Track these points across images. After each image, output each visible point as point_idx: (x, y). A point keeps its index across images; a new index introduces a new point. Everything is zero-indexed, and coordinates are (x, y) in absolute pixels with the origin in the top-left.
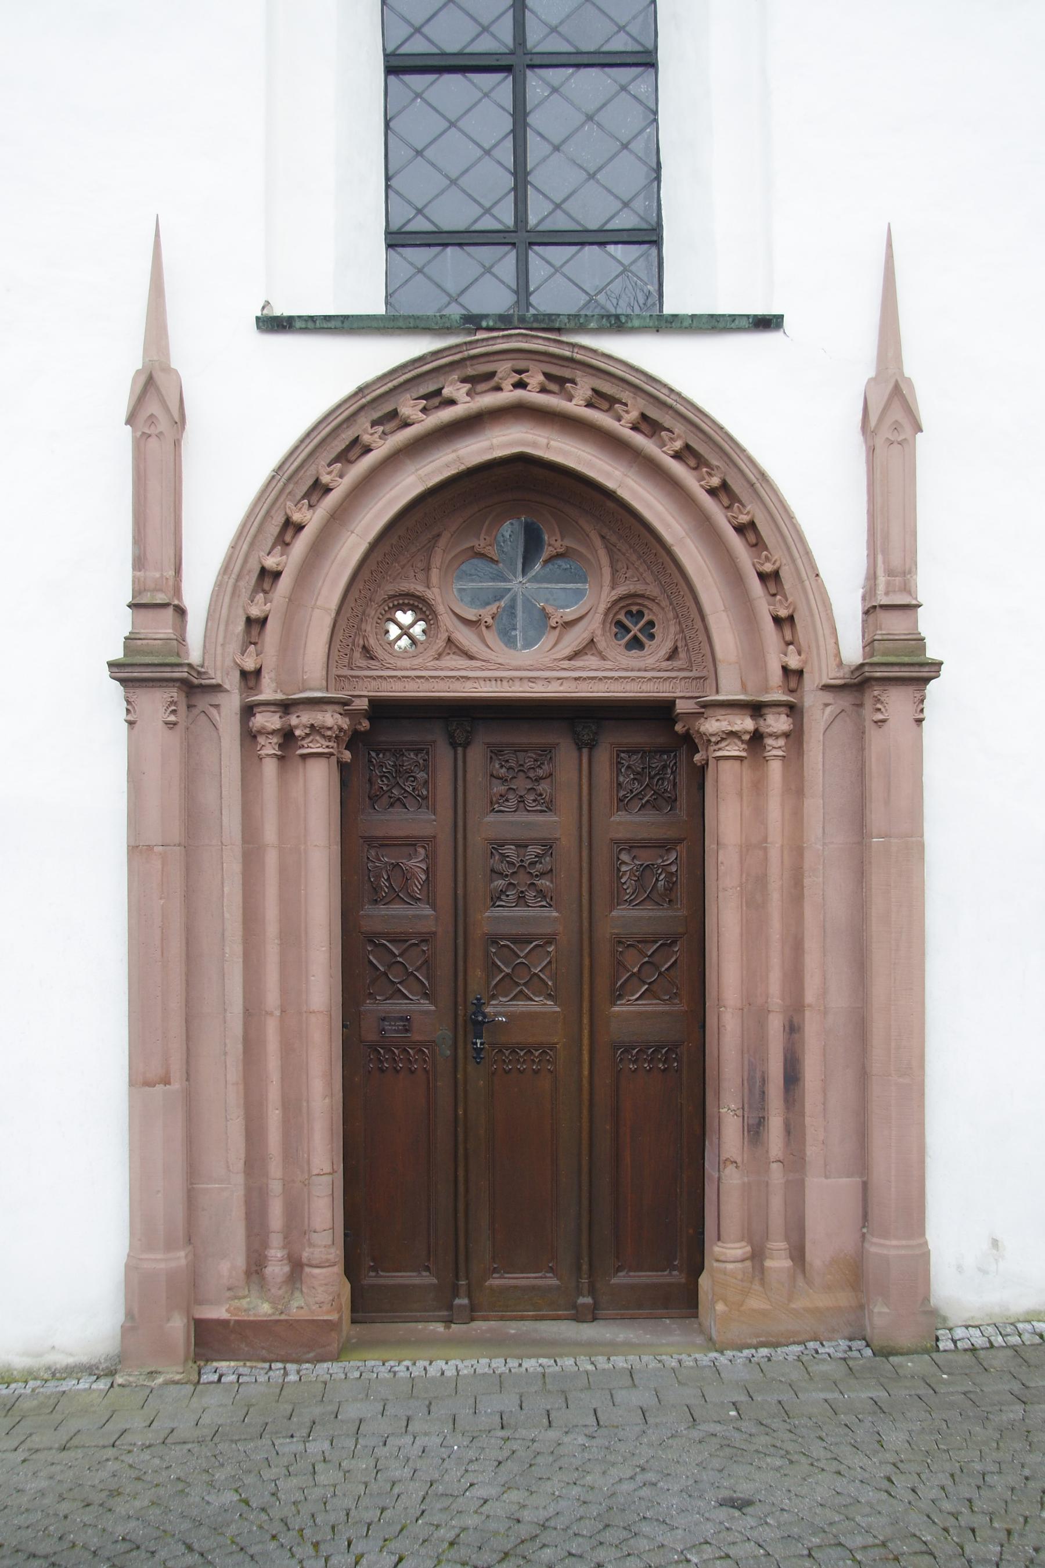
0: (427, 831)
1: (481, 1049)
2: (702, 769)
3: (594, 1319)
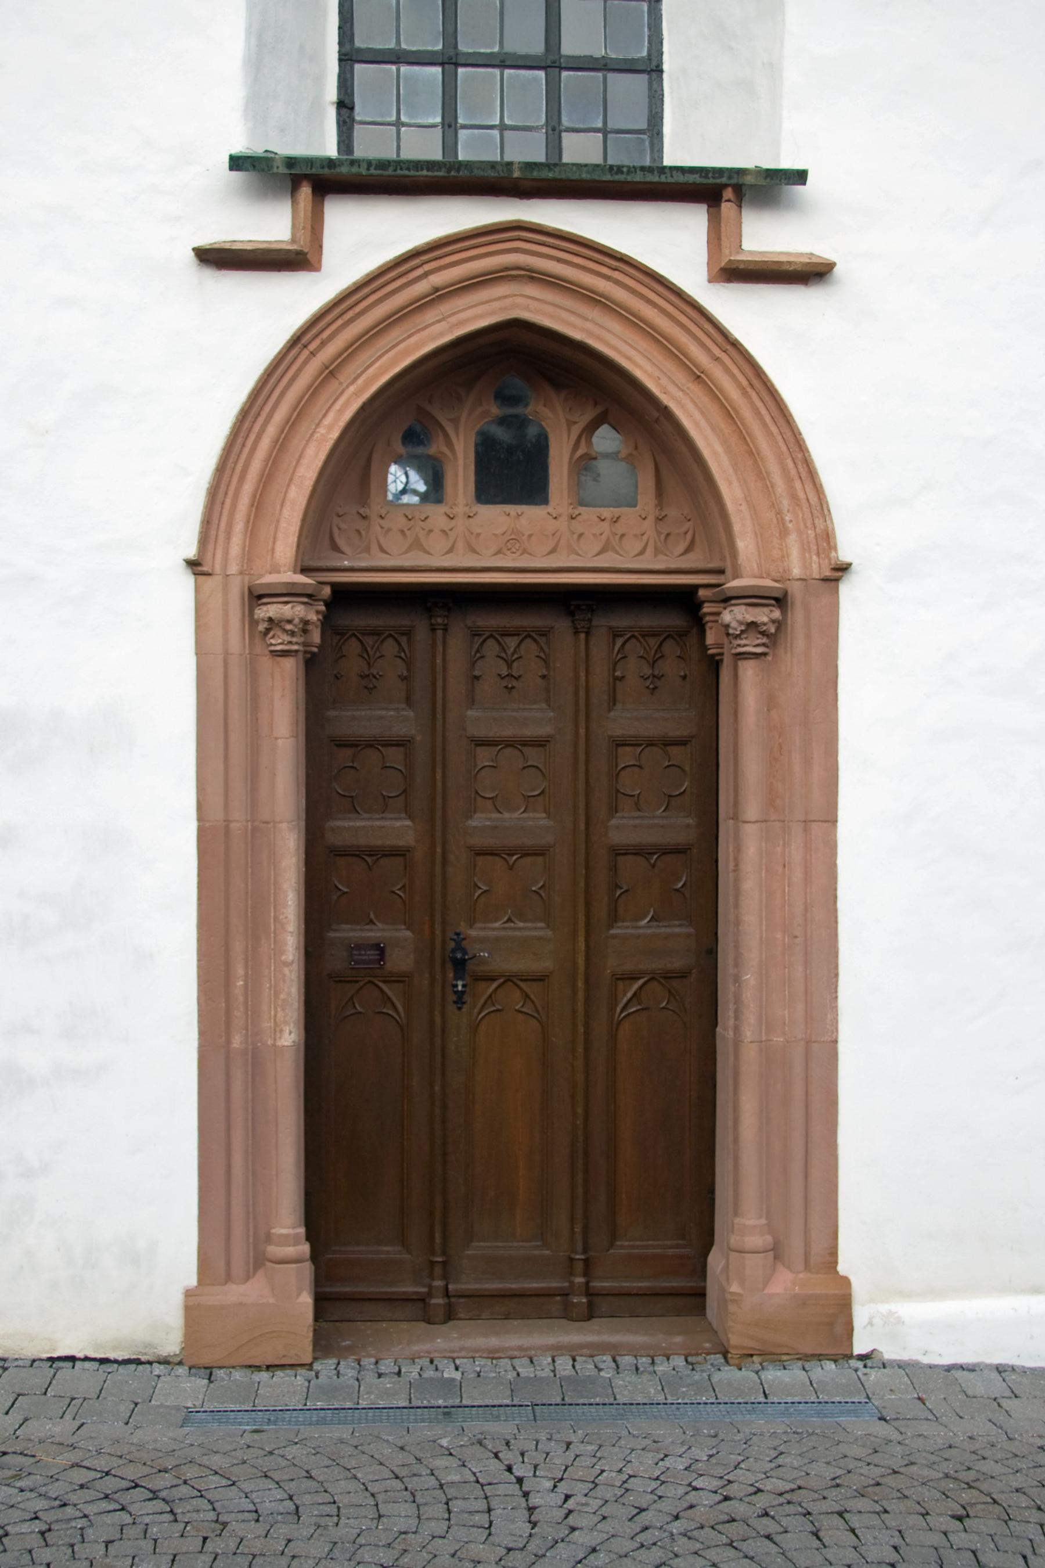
0: (401, 730)
1: (463, 992)
2: (714, 665)
3: (590, 1317)
